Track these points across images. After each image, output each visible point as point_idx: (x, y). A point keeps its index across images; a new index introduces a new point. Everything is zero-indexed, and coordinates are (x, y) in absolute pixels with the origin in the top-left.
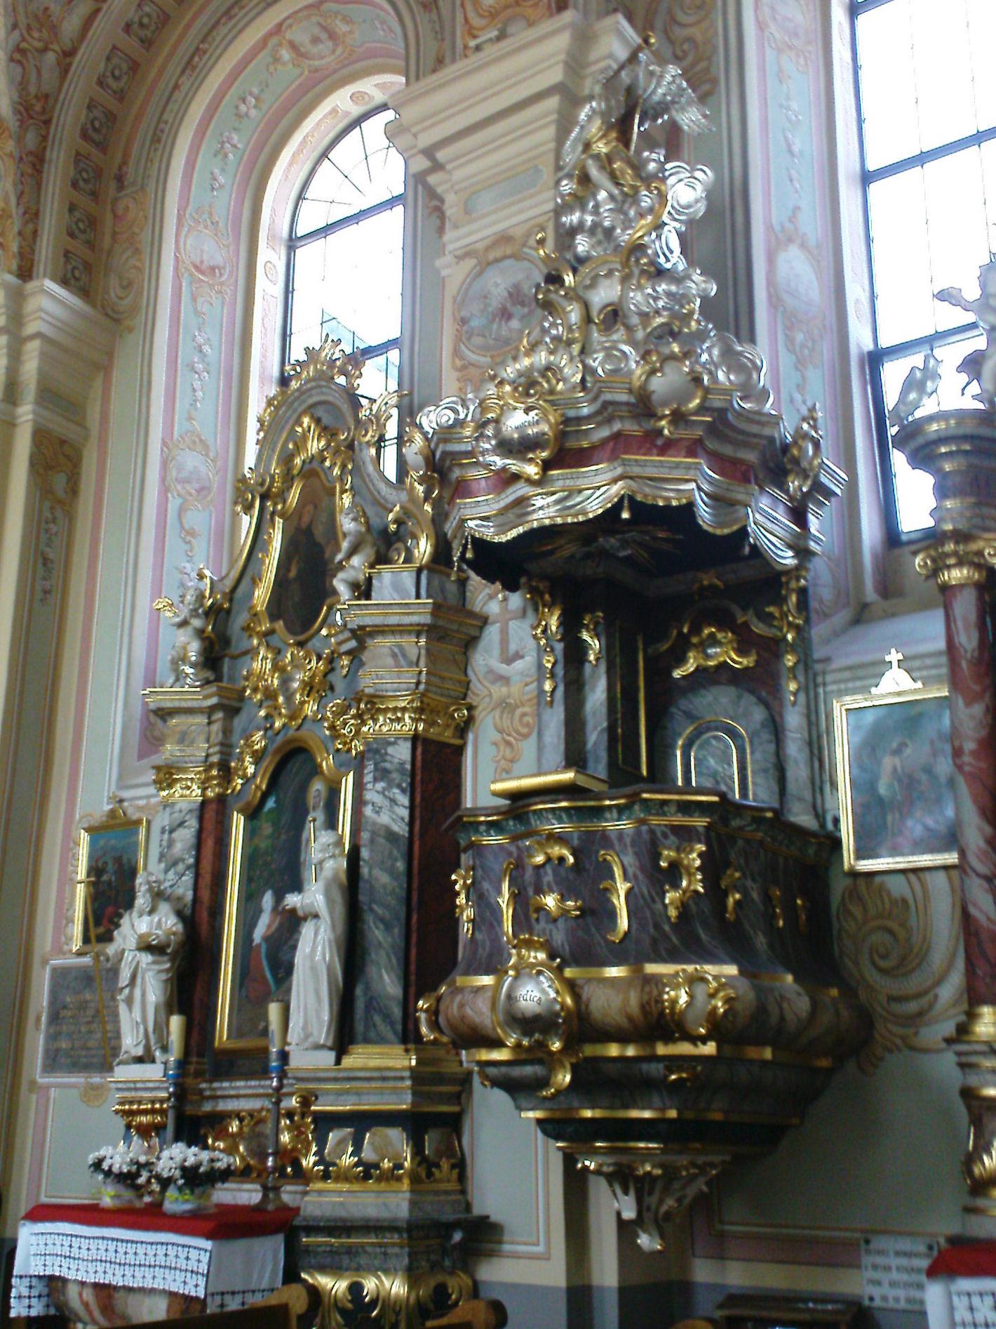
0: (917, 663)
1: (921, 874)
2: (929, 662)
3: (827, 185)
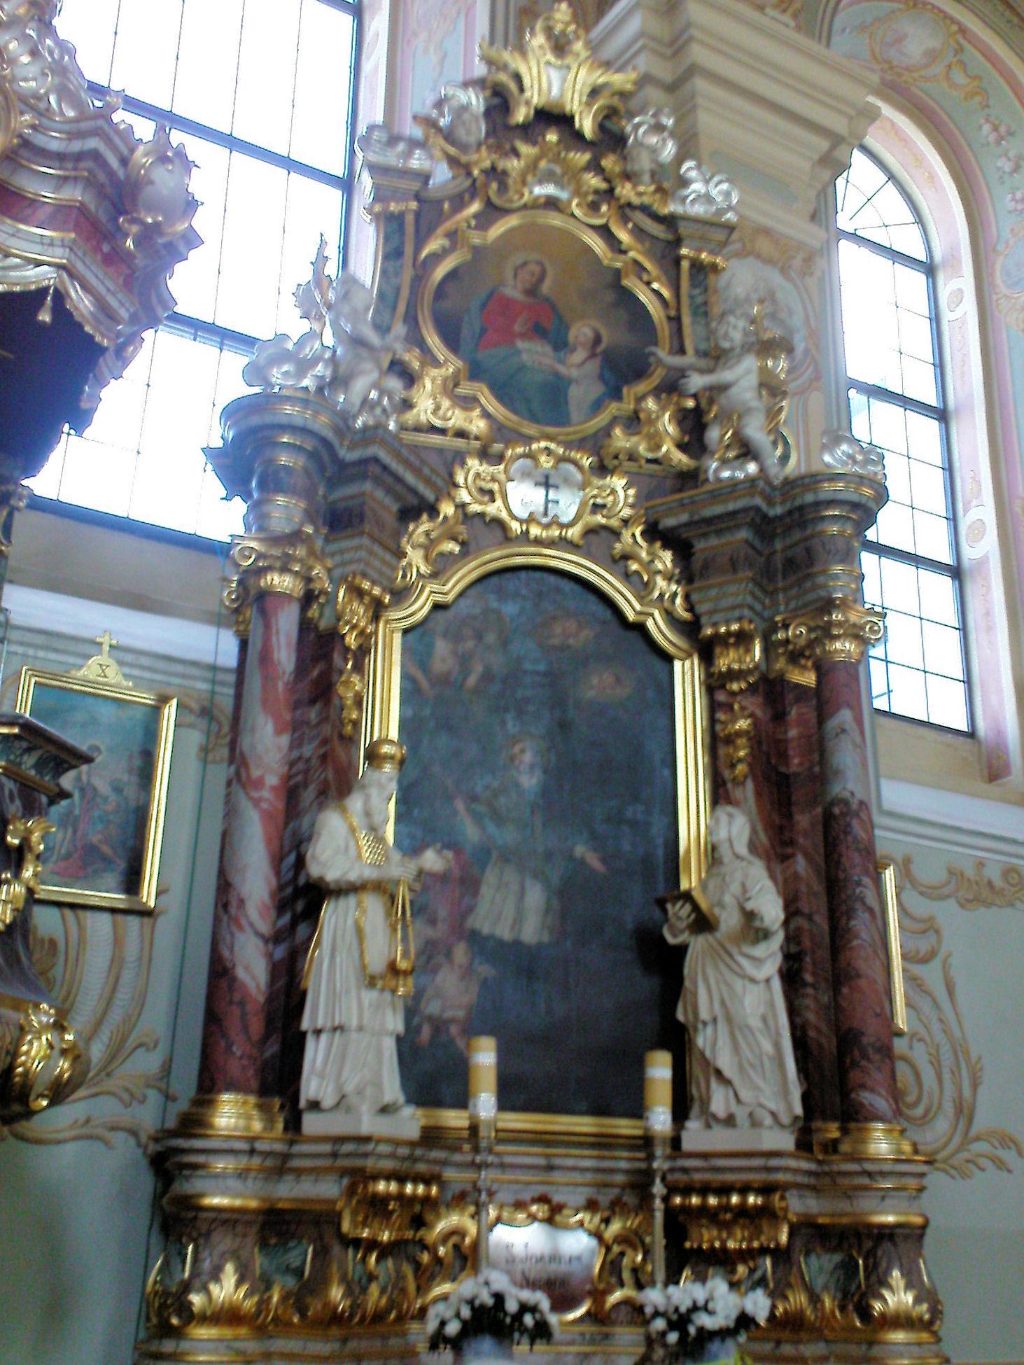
0: (129, 658)
1: (81, 913)
2: (144, 661)
3: (397, 115)
